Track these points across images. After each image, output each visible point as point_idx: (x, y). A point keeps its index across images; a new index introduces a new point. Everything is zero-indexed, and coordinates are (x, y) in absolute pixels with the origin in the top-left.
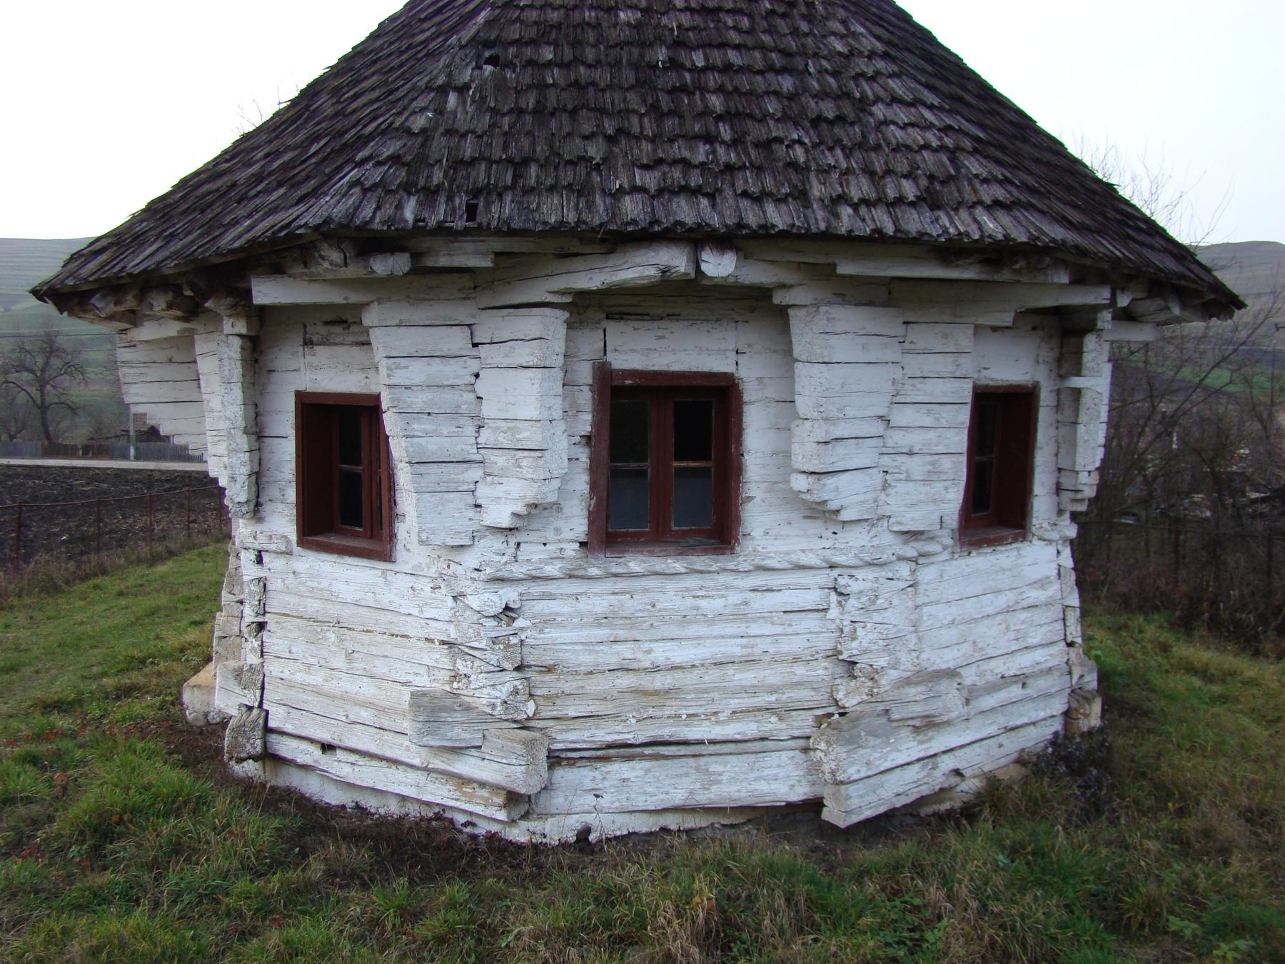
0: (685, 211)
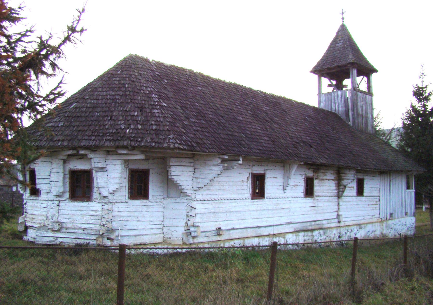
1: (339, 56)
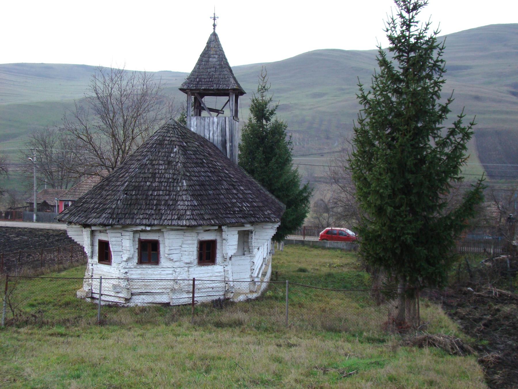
0: (144, 222)
1: (216, 76)
